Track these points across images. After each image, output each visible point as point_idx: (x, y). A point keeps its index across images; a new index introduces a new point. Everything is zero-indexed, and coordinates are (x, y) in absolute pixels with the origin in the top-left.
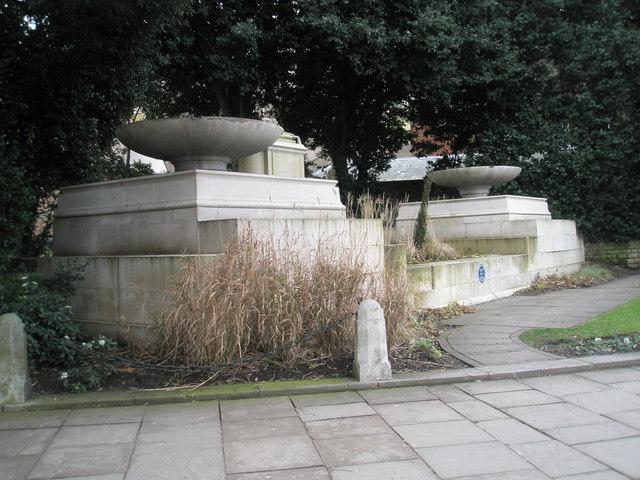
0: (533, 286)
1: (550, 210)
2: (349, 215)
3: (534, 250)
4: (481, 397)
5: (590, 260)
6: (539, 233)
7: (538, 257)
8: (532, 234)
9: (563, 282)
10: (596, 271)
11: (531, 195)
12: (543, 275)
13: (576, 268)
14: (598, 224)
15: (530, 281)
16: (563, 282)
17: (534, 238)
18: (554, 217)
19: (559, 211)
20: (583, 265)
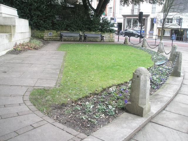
0: (14, 49)
1: (18, 14)
2: (19, 18)
3: (14, 31)
4: (176, 116)
5: (33, 36)
6: (16, 24)
7: (16, 34)
8: (13, 24)
9: (27, 47)
10: (37, 42)
11: (151, 25)
12: (18, 43)
13: (27, 40)
14: (35, 23)
15: (13, 46)
16: (27, 47)
17: (14, 26)
18: (19, 18)
19: (22, 15)
20: (31, 39)
